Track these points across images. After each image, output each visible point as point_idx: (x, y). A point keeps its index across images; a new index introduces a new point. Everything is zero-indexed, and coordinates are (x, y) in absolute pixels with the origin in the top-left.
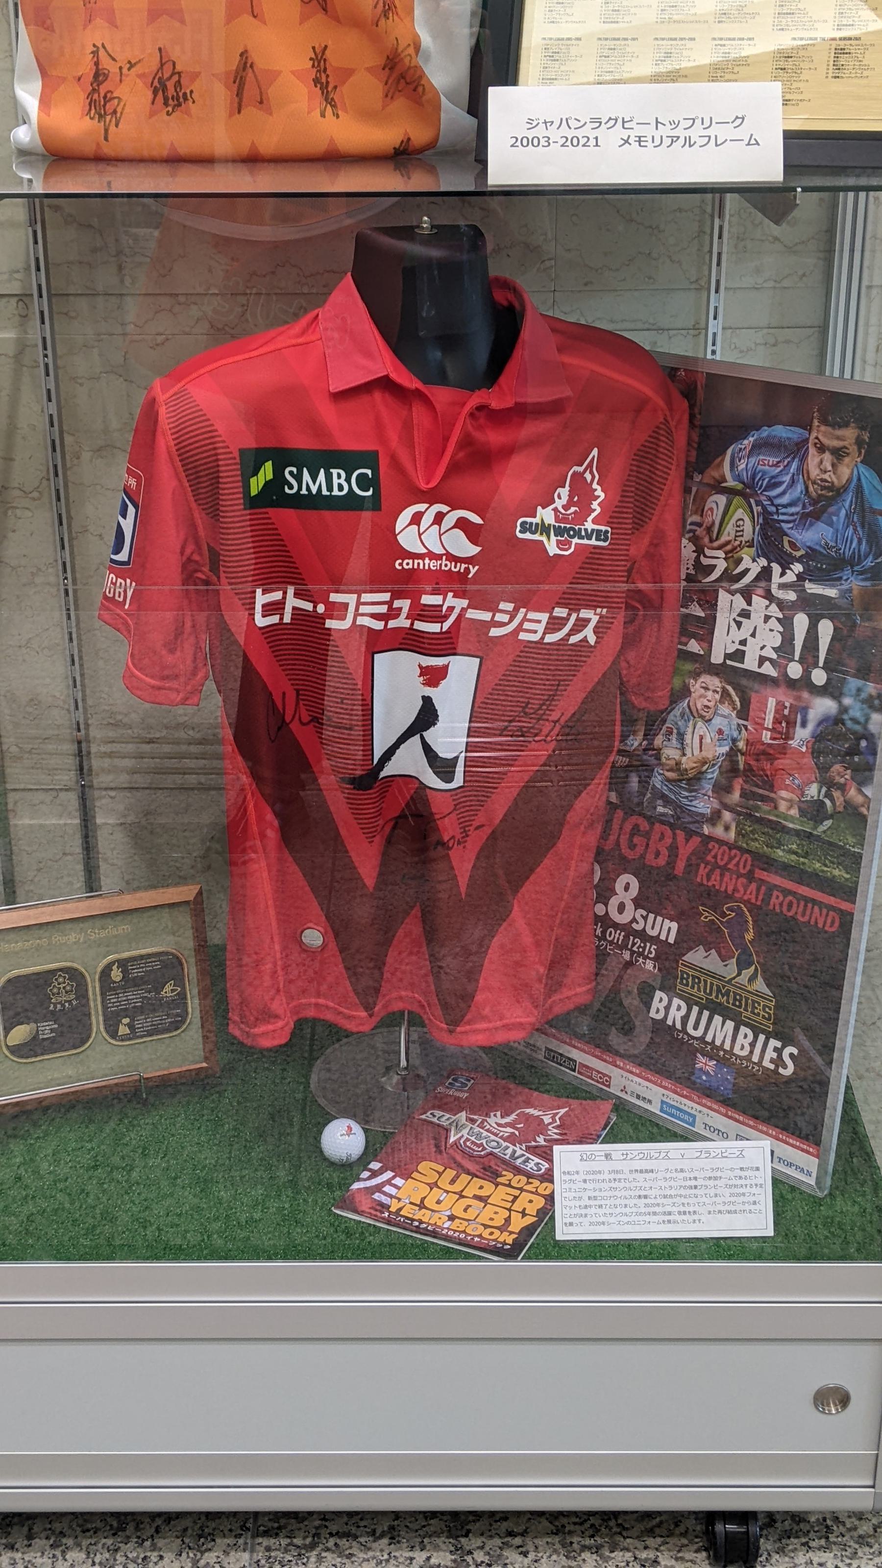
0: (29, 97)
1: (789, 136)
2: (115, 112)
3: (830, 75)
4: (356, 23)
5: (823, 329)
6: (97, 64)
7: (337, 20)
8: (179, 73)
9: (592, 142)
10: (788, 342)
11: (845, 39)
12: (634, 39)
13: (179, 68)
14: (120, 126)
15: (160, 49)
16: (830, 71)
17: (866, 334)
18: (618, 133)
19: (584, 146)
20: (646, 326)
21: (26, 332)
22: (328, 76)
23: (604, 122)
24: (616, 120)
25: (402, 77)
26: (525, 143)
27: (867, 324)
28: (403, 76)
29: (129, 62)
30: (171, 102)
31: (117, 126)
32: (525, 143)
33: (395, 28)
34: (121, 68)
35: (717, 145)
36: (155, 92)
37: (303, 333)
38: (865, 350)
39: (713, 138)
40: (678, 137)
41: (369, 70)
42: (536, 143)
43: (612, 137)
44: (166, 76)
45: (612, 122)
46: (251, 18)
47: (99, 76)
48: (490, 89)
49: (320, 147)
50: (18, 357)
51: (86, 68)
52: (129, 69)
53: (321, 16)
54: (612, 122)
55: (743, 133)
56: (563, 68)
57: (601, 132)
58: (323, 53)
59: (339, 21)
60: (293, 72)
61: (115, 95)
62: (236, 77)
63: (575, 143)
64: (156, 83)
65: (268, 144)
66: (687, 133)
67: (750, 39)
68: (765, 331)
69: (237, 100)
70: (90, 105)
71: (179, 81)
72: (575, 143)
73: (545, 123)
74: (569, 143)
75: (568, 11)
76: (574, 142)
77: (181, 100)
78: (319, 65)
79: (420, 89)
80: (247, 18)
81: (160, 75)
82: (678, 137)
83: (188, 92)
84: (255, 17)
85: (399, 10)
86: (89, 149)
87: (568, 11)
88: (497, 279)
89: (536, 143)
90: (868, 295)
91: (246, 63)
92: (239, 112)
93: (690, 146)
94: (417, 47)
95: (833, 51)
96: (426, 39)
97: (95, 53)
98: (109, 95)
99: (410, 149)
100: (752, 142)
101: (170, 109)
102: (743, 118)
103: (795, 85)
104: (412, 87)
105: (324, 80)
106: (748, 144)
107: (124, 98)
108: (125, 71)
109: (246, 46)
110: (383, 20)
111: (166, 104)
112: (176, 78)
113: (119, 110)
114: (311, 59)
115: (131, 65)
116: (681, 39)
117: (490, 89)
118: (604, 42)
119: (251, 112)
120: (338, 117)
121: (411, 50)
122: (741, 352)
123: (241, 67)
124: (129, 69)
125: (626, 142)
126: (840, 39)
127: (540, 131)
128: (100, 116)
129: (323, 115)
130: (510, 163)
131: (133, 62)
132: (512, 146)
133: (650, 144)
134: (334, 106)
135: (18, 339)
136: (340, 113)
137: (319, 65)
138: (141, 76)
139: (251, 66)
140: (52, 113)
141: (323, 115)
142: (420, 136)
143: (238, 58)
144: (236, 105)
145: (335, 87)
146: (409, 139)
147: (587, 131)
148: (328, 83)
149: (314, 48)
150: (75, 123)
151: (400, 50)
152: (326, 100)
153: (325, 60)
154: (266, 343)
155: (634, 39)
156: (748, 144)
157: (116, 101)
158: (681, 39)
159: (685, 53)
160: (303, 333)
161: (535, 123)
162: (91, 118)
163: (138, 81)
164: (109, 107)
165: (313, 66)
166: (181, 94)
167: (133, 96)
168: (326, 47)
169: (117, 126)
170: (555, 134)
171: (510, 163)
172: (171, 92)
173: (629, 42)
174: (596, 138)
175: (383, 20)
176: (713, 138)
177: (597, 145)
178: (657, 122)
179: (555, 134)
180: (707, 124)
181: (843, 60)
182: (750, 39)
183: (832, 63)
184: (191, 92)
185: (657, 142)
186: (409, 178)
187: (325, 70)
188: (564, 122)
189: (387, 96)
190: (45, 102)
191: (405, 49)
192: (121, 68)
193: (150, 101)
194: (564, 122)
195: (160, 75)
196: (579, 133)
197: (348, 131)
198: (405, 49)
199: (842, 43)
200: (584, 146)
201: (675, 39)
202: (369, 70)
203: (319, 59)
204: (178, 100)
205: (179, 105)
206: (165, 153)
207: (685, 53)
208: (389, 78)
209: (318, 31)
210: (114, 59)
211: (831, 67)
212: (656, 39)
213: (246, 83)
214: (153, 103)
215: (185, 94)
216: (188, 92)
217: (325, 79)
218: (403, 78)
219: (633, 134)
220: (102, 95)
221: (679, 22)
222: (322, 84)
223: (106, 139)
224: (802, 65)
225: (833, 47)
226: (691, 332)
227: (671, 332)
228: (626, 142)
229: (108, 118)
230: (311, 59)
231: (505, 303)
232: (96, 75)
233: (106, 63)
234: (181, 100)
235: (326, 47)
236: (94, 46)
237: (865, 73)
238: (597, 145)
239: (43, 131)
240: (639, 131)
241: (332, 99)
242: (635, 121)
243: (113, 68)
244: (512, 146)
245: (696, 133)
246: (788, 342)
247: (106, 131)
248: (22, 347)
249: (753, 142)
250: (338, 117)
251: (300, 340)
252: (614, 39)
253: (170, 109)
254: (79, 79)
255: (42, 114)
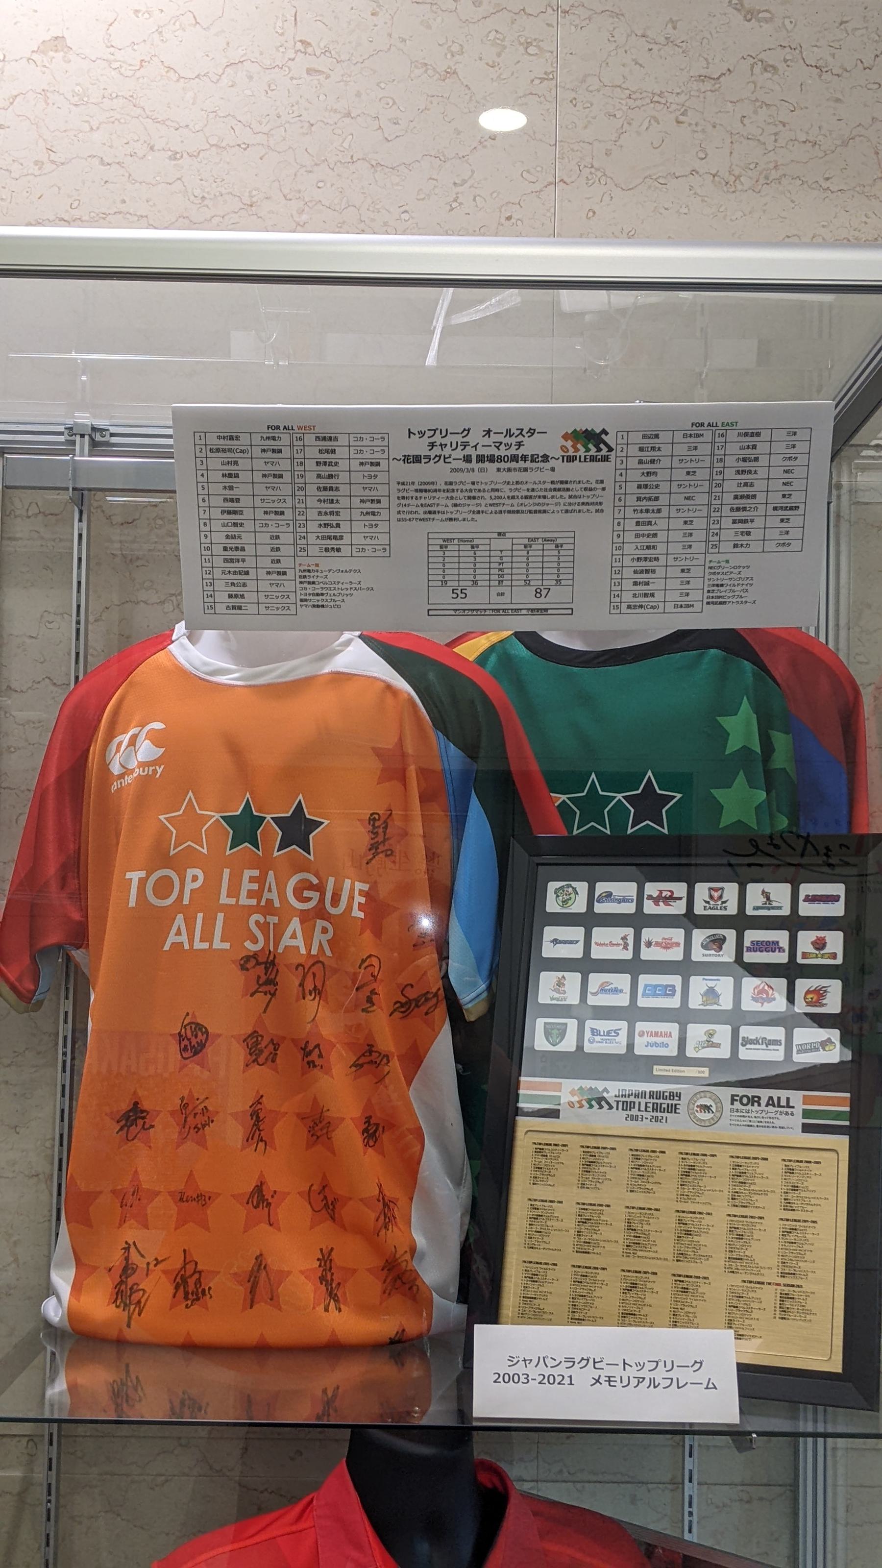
0: (63, 1280)
1: (742, 1368)
2: (139, 1302)
3: (778, 1316)
4: (359, 1230)
5: (794, 1487)
6: (127, 1259)
7: (343, 1227)
8: (200, 1272)
9: (567, 1381)
10: (761, 1499)
11: (788, 1285)
12: (603, 1269)
13: (199, 1267)
14: (142, 1315)
15: (185, 1251)
16: (778, 1312)
17: (835, 1494)
18: (591, 1372)
19: (559, 1383)
20: (626, 1479)
21: (32, 1471)
22: (333, 1274)
23: (577, 1361)
24: (588, 1360)
25: (399, 1278)
26: (506, 1379)
27: (835, 1486)
28: (399, 1277)
29: (156, 1259)
30: (190, 1296)
31: (139, 1315)
32: (506, 1379)
33: (393, 1237)
34: (148, 1264)
35: (679, 1388)
36: (177, 1288)
37: (299, 1518)
38: (835, 1509)
39: (675, 1381)
40: (644, 1379)
41: (369, 1270)
42: (516, 1379)
43: (583, 1376)
44: (188, 1274)
45: (584, 1362)
46: (267, 1227)
47: (128, 1269)
48: (476, 1326)
49: (324, 1337)
50: (22, 1496)
51: (116, 1259)
52: (155, 1265)
53: (329, 1223)
54: (584, 1362)
55: (702, 1376)
56: (541, 1289)
57: (575, 1371)
58: (330, 1254)
59: (345, 1229)
60: (302, 1272)
61: (141, 1287)
62: (250, 1277)
63: (551, 1381)
64: (178, 1279)
65: (275, 1334)
66: (652, 1375)
67: (705, 1278)
68: (740, 1488)
69: (250, 1297)
70: (117, 1294)
71: (199, 1279)
72: (551, 1381)
73: (525, 1360)
74: (546, 1381)
75: (545, 1239)
76: (550, 1380)
77: (200, 1295)
78: (325, 1265)
79: (415, 1288)
80: (264, 1226)
81: (183, 1272)
82: (644, 1379)
83: (207, 1289)
84: (271, 1225)
85: (398, 1219)
86: (113, 1333)
87: (545, 1239)
88: (482, 1463)
89: (516, 1379)
90: (834, 1456)
91: (260, 1265)
92: (251, 1307)
93: (655, 1387)
94: (413, 1250)
95: (779, 1295)
96: (420, 1240)
97: (127, 1249)
98: (135, 1287)
99: (404, 1339)
100: (710, 1386)
101: (189, 1302)
102: (701, 1363)
103: (747, 1322)
104: (408, 1286)
105: (329, 1278)
106: (707, 1388)
107: (148, 1291)
108: (151, 1266)
109: (261, 1251)
110: (384, 1231)
111: (186, 1298)
112: (197, 1276)
113: (143, 1300)
114: (318, 1259)
115: (158, 1262)
116: (645, 1273)
117: (476, 1326)
118: (578, 1269)
119: (261, 1307)
120: (340, 1311)
121: (407, 1257)
122: (717, 1507)
123: (256, 1268)
124: (155, 1265)
125: (597, 1381)
126: (784, 1285)
127: (520, 1369)
128: (125, 1305)
129: (326, 1310)
130: (490, 1400)
131: (160, 1259)
132: (495, 1382)
133: (618, 1384)
134: (337, 1301)
135: (24, 1479)
136: (342, 1307)
137: (325, 1265)
138: (165, 1272)
139: (265, 1268)
140: (82, 1298)
141: (326, 1310)
142: (413, 1326)
143: (254, 1261)
144: (249, 1301)
145: (339, 1284)
146: (404, 1330)
147: (562, 1370)
148: (332, 1280)
149: (321, 1250)
150: (100, 1308)
151: (397, 1256)
152: (330, 1295)
153: (331, 1260)
154: (260, 1531)
155: (603, 1269)
156: (707, 1388)
157: (141, 1293)
158: (645, 1273)
159: (649, 1285)
160: (299, 1518)
161: (515, 1361)
162: (117, 1307)
163: (163, 1276)
164: (135, 1297)
165: (320, 1266)
166: (200, 1290)
167: (156, 1289)
168: (332, 1249)
169: (139, 1315)
170: (534, 1372)
171: (490, 1400)
172: (191, 1288)
173: (599, 1271)
174: (570, 1377)
175: (384, 1231)
176: (675, 1381)
177: (571, 1384)
178: (625, 1363)
179: (534, 1372)
180: (669, 1367)
181: (787, 1304)
182: (705, 1278)
183: (778, 1306)
184: (210, 1288)
185: (625, 1382)
186: (403, 1365)
187: (331, 1268)
188: (542, 1360)
189: (384, 1292)
190: (77, 1288)
191: (402, 1255)
192: (148, 1264)
193: (171, 1296)
194: (542, 1360)
195: (183, 1272)
196: (555, 1372)
197: (346, 1323)
198: (402, 1255)
199: (786, 1288)
200: (559, 1383)
201: (640, 1272)
202: (369, 1270)
203: (326, 1260)
204: (197, 1295)
205: (198, 1299)
206: (181, 1340)
207: (649, 1285)
208: (387, 1277)
209: (325, 1235)
210: (143, 1256)
211: (778, 1309)
212: (623, 1271)
213: (258, 1283)
214: (174, 1297)
215: (204, 1290)
216: (207, 1289)
217: (330, 1278)
218: (400, 1278)
219: (603, 1374)
220: (129, 1287)
221: (642, 1257)
222: (327, 1281)
223: (129, 1326)
224: (752, 1305)
225: (779, 1292)
226: (670, 1486)
227: (650, 1486)
228: (597, 1381)
229: (132, 1307)
230: (318, 1259)
231: (489, 1485)
232: (125, 1269)
233: (134, 1257)
234: (200, 1295)
235: (332, 1249)
236: (126, 1243)
237: (808, 1317)
238: (571, 1384)
239: (71, 1315)
240: (609, 1371)
241: (336, 1295)
242: (605, 1362)
243: (141, 1263)
244: (495, 1382)
245: (660, 1374)
246: (761, 1499)
247: (130, 1318)
248: (27, 1484)
249: (711, 1386)
250: (340, 1311)
251: (294, 1528)
252: (586, 1267)
253: (189, 1302)
254: (110, 1270)
255: (73, 1300)
